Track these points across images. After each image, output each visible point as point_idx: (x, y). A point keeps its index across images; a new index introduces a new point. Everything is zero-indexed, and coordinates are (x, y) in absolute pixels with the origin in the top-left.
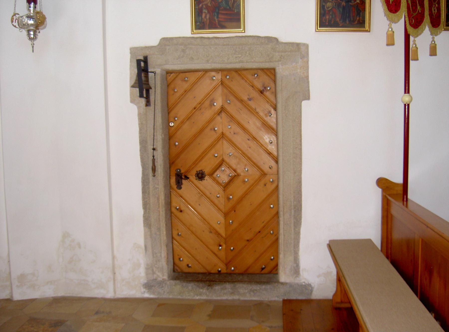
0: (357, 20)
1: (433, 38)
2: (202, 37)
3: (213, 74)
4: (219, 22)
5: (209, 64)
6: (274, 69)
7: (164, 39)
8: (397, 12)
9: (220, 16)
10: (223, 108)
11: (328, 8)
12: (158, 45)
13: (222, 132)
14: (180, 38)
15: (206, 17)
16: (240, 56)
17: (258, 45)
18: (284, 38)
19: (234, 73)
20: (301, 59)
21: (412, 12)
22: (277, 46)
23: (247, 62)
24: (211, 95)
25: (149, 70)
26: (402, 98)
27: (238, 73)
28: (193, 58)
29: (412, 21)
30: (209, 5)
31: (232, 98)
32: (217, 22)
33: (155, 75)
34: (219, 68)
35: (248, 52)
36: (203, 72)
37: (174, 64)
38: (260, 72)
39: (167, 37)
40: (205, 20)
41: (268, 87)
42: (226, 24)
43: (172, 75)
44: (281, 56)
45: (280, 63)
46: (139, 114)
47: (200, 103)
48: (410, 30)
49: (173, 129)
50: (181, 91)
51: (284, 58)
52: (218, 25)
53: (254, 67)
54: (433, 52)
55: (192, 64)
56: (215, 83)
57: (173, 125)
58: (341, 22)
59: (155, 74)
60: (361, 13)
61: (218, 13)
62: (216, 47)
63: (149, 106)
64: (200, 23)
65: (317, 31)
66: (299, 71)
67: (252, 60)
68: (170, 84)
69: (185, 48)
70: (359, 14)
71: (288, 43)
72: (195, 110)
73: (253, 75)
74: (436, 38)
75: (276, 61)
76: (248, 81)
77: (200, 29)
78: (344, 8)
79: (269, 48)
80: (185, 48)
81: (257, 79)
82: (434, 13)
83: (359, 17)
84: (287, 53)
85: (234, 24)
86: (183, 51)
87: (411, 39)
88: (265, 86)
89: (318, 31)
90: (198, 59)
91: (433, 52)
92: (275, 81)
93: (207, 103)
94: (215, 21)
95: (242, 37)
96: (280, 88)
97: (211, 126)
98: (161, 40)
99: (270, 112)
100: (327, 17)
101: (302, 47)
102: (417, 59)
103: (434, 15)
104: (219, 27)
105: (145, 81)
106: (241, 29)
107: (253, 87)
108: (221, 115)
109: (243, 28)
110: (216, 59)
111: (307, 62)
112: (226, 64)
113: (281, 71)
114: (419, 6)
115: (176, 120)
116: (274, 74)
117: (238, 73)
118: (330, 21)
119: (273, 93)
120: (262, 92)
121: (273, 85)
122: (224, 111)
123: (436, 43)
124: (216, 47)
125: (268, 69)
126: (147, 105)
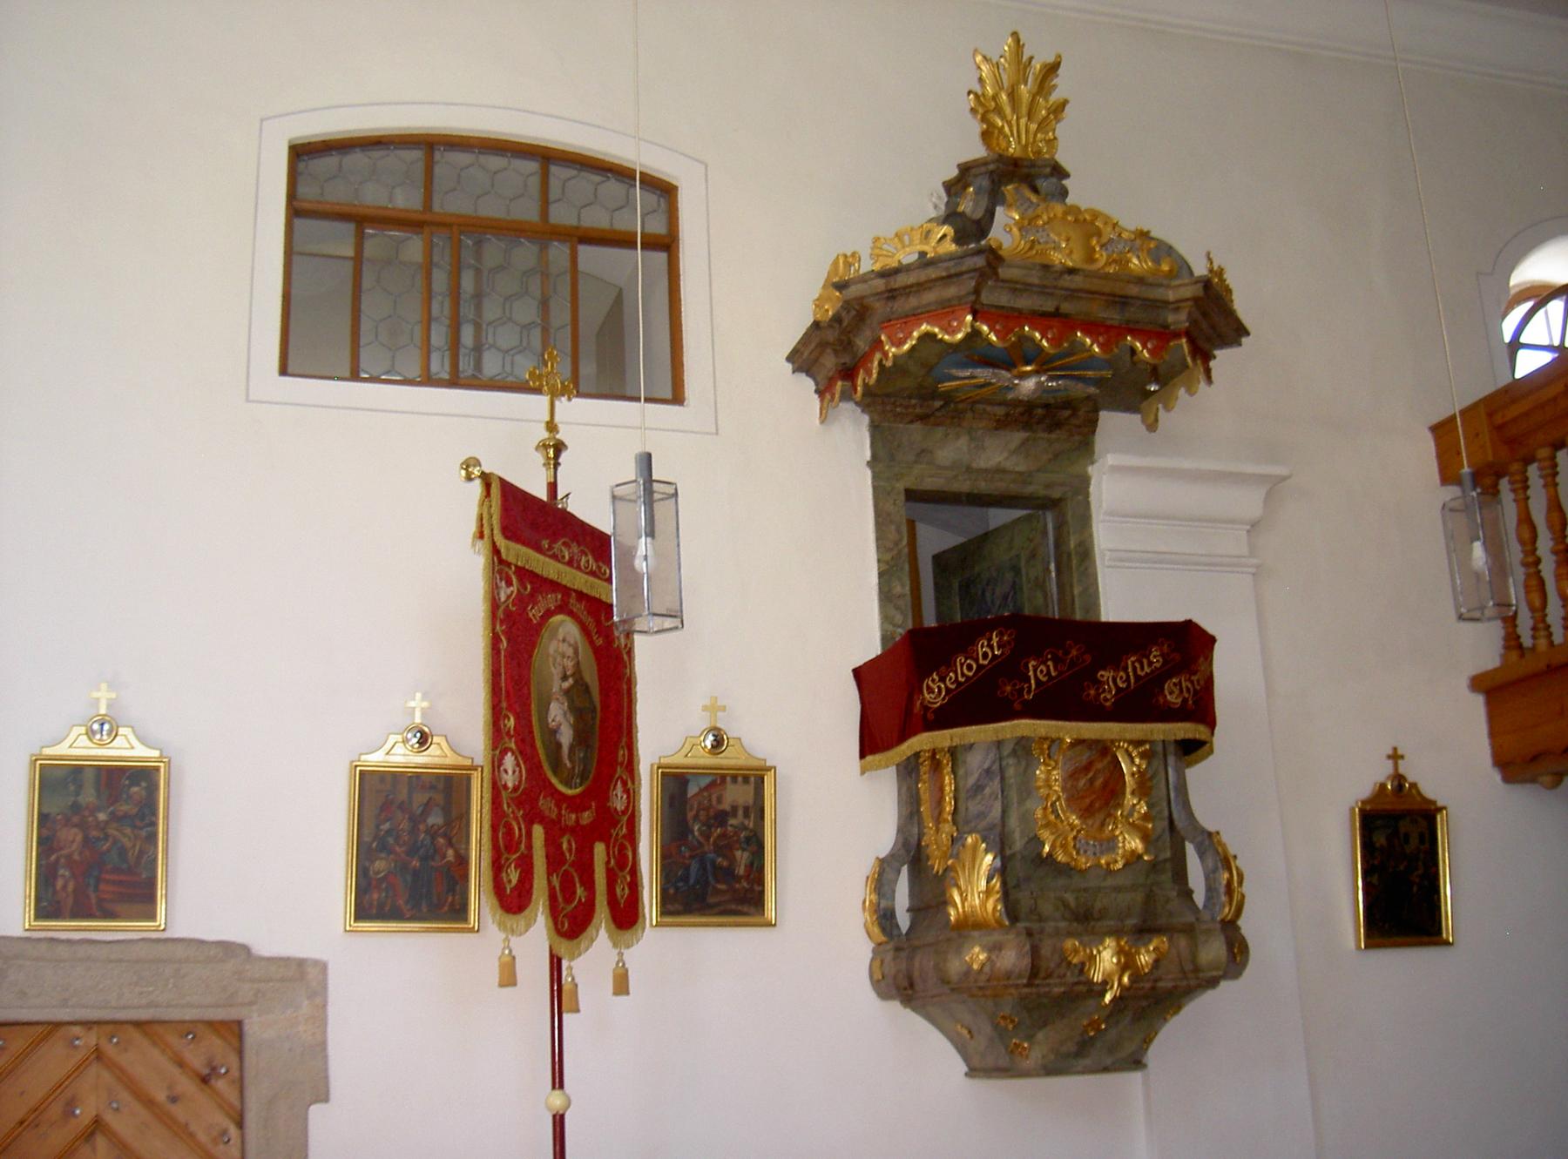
0: (447, 904)
1: (621, 954)
2: (52, 940)
3: (76, 1030)
5: (68, 1010)
6: (239, 1023)
8: (526, 908)
9: (102, 887)
11: (378, 873)
15: (65, 887)
16: (151, 989)
18: (268, 943)
19: (135, 1035)
21: (562, 905)
22: (248, 967)
24: (66, 1087)
26: (546, 1103)
29: (563, 924)
30: (76, 857)
31: (125, 1096)
41: (222, 1066)
45: (255, 1007)
48: (563, 947)
53: (187, 1018)
54: (621, 985)
56: (79, 1056)
58: (409, 907)
60: (458, 887)
61: (98, 880)
65: (349, 931)
66: (301, 1028)
70: (452, 890)
73: (182, 1037)
74: (628, 954)
78: (415, 873)
81: (192, 1046)
82: (622, 897)
83: (454, 896)
87: (565, 964)
88: (214, 1064)
89: (351, 929)
91: (621, 985)
92: (240, 1053)
93: (56, 1110)
95: (158, 941)
99: (224, 1132)
100: (375, 896)
102: (578, 1011)
103: (623, 901)
111: (324, 1006)
113: (256, 1030)
114: (581, 886)
118: (381, 906)
119: (233, 1082)
120: (205, 1080)
121: (233, 1059)
123: (627, 966)
125: (223, 1023)
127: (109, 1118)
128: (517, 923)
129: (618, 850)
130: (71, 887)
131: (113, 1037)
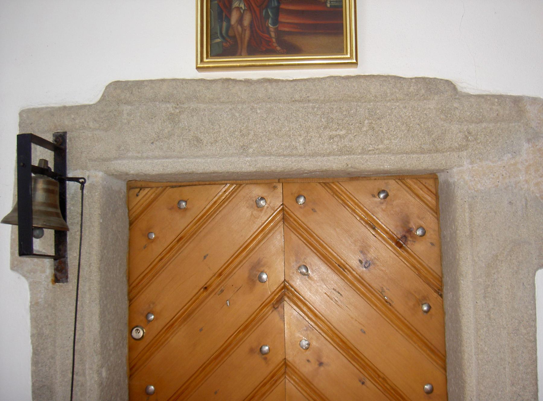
2: (228, 80)
3: (257, 191)
4: (278, 33)
5: (249, 159)
7: (116, 85)
9: (283, 19)
10: (288, 289)
12: (99, 102)
13: (285, 359)
14: (163, 80)
15: (240, 21)
16: (342, 133)
17: (397, 100)
20: (529, 141)
23: (364, 152)
25: (70, 175)
27: (331, 189)
28: (199, 140)
32: (273, 34)
33: (82, 188)
34: (279, 170)
35: (366, 122)
36: (232, 184)
37: (141, 158)
38: (393, 186)
39: (127, 80)
40: (240, 28)
42: (298, 41)
43: (143, 193)
44: (467, 134)
45: (465, 153)
46: (35, 305)
47: (220, 275)
49: (142, 345)
50: (171, 237)
51: (476, 139)
52: (275, 45)
55: (198, 157)
56: (263, 218)
57: (143, 336)
59: (83, 184)
62: (269, 106)
63: (63, 282)
64: (223, 37)
66: (522, 177)
67: (380, 146)
68: (136, 218)
69: (177, 111)
71: (487, 95)
72: (205, 294)
73: (374, 196)
75: (451, 149)
76: (358, 211)
77: (223, 54)
79: (429, 108)
80: (177, 111)
81: (383, 207)
84: (484, 125)
85: (323, 40)
86: (172, 118)
90: (216, 141)
94: (269, 32)
96: (468, 232)
97: (251, 340)
98: (108, 87)
101: (528, 107)
104: (278, 48)
105: (44, 204)
106: (347, 54)
107: (374, 229)
108: (279, 309)
109: (351, 50)
110: (270, 142)
112: (300, 158)
115: (149, 321)
116: (433, 190)
117: (331, 189)
121: (429, 221)
122: (289, 298)
124: (269, 106)
126: (56, 280)
127: (298, 283)
128: (272, 312)
129: (292, 290)
130: (246, 22)
131: (299, 197)
